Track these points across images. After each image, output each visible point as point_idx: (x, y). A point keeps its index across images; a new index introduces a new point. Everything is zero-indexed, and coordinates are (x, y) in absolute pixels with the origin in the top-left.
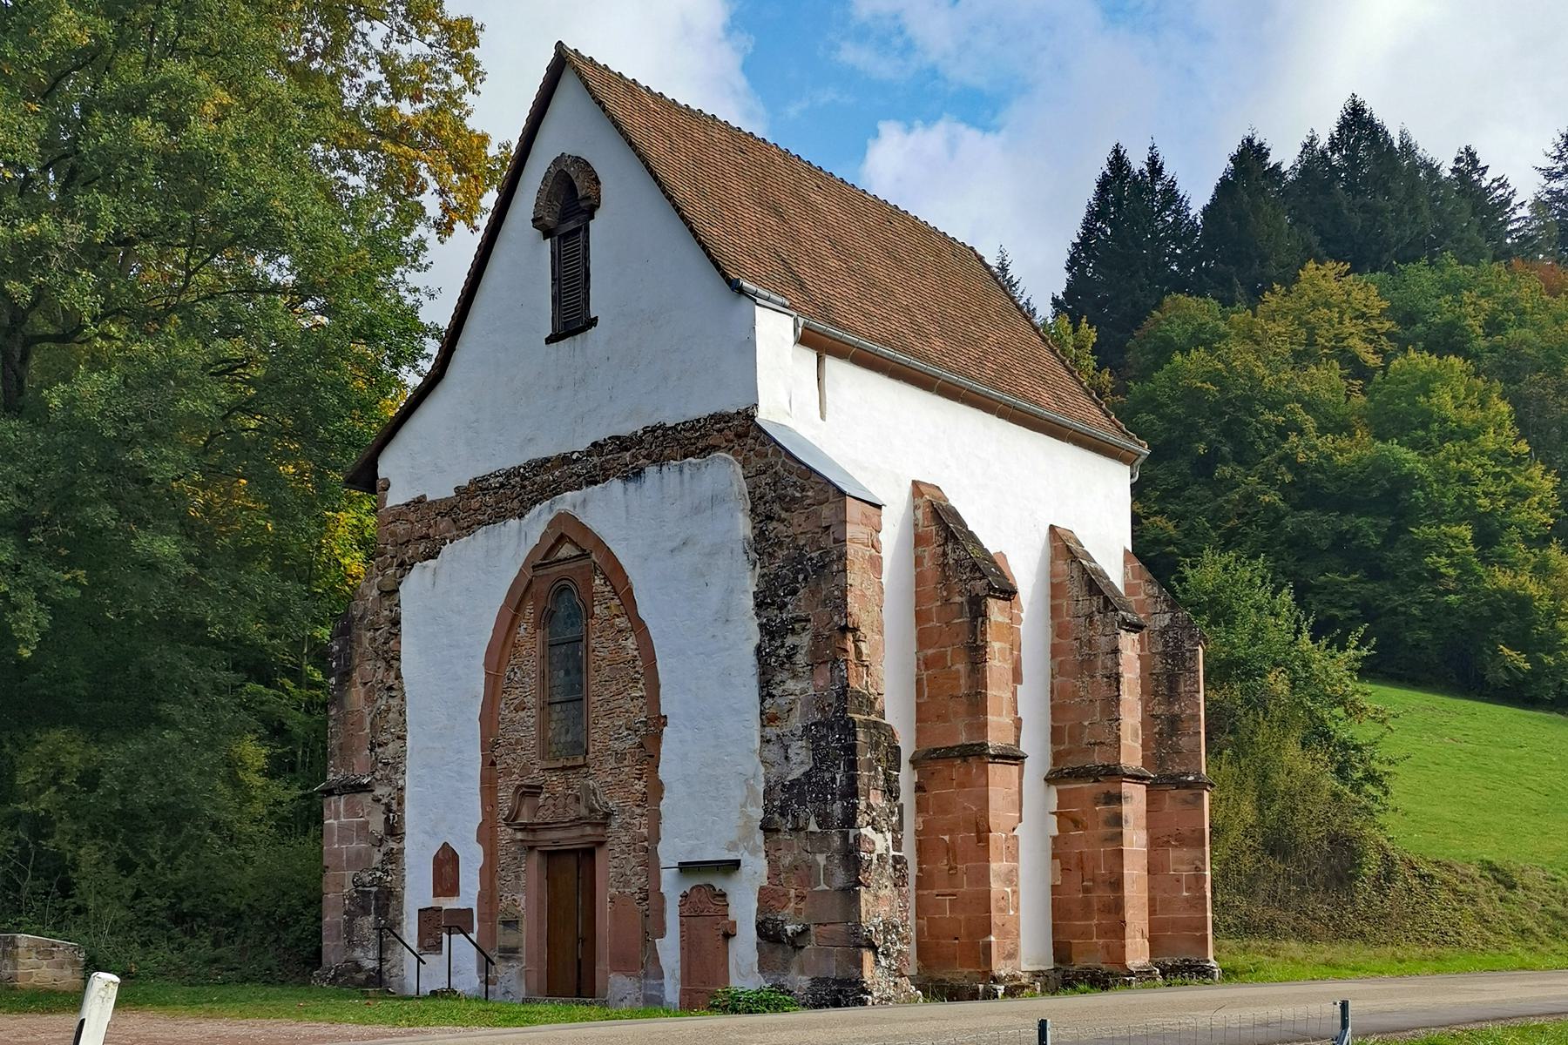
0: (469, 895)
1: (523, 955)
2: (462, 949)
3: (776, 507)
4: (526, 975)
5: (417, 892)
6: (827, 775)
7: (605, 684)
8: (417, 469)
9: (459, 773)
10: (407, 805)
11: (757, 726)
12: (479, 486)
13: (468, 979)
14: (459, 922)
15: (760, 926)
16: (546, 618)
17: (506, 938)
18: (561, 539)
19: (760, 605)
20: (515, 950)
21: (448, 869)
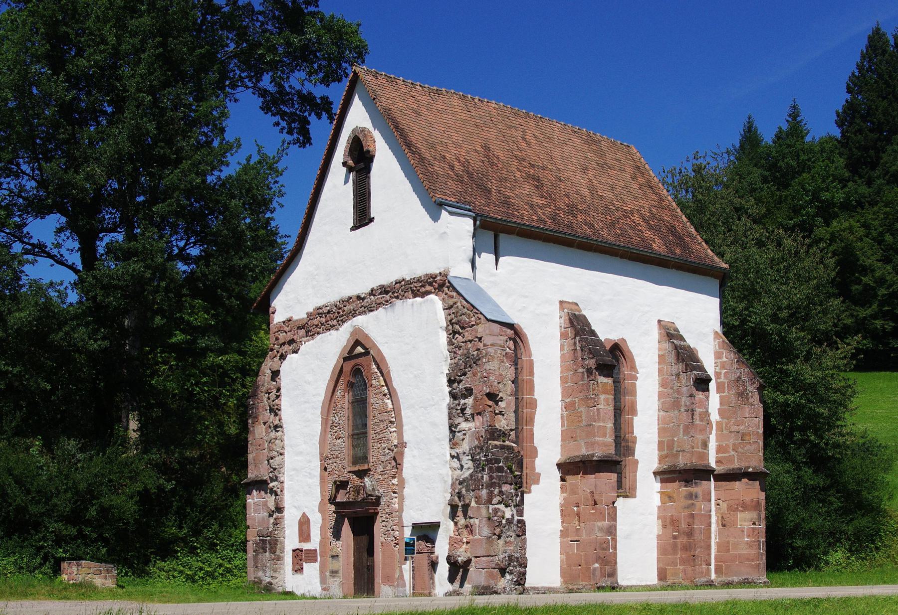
0: (314, 544)
1: (340, 574)
2: (312, 569)
3: (457, 327)
4: (342, 584)
5: (290, 540)
6: (480, 475)
7: (376, 424)
8: (291, 302)
9: (310, 474)
10: (285, 491)
11: (448, 448)
12: (319, 312)
13: (315, 588)
14: (311, 556)
15: (449, 559)
16: (351, 385)
17: (333, 565)
18: (357, 343)
19: (451, 382)
20: (336, 572)
21: (305, 527)
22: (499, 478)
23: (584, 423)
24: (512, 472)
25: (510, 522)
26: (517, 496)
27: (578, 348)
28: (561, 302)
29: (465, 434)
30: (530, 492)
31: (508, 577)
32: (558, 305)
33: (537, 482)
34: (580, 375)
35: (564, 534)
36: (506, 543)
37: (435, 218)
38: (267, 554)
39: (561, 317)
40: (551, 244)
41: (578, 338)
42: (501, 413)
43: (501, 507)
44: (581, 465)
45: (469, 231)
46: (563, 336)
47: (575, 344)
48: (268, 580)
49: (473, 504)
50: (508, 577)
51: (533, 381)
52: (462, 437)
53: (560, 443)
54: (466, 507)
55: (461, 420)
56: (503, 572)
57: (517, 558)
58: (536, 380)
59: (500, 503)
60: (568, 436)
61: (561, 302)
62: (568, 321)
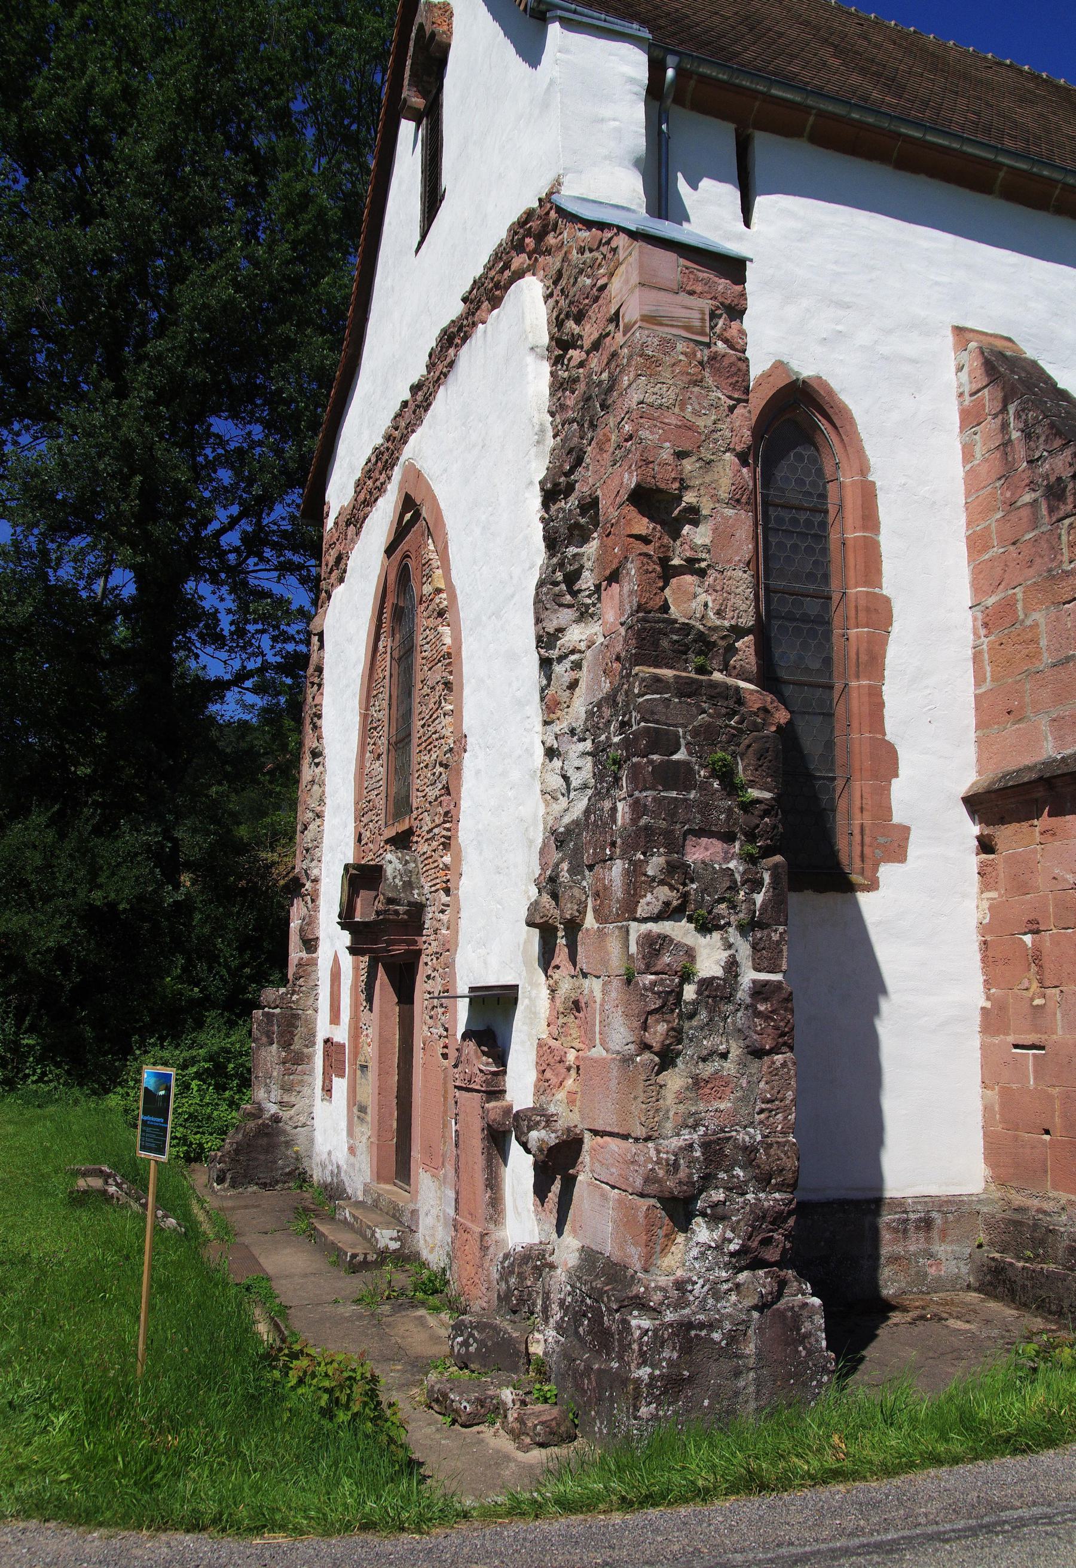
11: (539, 727)
22: (671, 809)
23: (1047, 659)
24: (731, 787)
25: (715, 992)
26: (756, 885)
27: (1015, 435)
28: (959, 330)
29: (577, 666)
30: (873, 886)
31: (703, 1233)
32: (950, 339)
33: (899, 854)
34: (1025, 513)
35: (992, 1021)
36: (697, 1083)
37: (531, 52)
38: (275, 1046)
39: (960, 369)
40: (922, 178)
41: (1012, 409)
42: (692, 566)
43: (681, 931)
44: (1040, 793)
45: (632, 80)
46: (970, 418)
47: (1005, 426)
48: (273, 1109)
49: (590, 921)
50: (703, 1233)
51: (876, 545)
52: (567, 678)
53: (972, 735)
54: (573, 927)
55: (566, 615)
56: (680, 1210)
57: (750, 1150)
58: (887, 542)
59: (667, 913)
60: (996, 711)
61: (959, 330)
62: (980, 372)
